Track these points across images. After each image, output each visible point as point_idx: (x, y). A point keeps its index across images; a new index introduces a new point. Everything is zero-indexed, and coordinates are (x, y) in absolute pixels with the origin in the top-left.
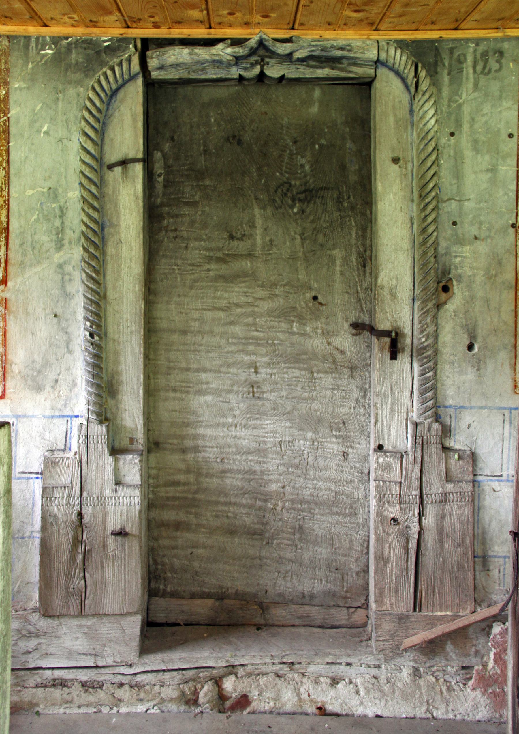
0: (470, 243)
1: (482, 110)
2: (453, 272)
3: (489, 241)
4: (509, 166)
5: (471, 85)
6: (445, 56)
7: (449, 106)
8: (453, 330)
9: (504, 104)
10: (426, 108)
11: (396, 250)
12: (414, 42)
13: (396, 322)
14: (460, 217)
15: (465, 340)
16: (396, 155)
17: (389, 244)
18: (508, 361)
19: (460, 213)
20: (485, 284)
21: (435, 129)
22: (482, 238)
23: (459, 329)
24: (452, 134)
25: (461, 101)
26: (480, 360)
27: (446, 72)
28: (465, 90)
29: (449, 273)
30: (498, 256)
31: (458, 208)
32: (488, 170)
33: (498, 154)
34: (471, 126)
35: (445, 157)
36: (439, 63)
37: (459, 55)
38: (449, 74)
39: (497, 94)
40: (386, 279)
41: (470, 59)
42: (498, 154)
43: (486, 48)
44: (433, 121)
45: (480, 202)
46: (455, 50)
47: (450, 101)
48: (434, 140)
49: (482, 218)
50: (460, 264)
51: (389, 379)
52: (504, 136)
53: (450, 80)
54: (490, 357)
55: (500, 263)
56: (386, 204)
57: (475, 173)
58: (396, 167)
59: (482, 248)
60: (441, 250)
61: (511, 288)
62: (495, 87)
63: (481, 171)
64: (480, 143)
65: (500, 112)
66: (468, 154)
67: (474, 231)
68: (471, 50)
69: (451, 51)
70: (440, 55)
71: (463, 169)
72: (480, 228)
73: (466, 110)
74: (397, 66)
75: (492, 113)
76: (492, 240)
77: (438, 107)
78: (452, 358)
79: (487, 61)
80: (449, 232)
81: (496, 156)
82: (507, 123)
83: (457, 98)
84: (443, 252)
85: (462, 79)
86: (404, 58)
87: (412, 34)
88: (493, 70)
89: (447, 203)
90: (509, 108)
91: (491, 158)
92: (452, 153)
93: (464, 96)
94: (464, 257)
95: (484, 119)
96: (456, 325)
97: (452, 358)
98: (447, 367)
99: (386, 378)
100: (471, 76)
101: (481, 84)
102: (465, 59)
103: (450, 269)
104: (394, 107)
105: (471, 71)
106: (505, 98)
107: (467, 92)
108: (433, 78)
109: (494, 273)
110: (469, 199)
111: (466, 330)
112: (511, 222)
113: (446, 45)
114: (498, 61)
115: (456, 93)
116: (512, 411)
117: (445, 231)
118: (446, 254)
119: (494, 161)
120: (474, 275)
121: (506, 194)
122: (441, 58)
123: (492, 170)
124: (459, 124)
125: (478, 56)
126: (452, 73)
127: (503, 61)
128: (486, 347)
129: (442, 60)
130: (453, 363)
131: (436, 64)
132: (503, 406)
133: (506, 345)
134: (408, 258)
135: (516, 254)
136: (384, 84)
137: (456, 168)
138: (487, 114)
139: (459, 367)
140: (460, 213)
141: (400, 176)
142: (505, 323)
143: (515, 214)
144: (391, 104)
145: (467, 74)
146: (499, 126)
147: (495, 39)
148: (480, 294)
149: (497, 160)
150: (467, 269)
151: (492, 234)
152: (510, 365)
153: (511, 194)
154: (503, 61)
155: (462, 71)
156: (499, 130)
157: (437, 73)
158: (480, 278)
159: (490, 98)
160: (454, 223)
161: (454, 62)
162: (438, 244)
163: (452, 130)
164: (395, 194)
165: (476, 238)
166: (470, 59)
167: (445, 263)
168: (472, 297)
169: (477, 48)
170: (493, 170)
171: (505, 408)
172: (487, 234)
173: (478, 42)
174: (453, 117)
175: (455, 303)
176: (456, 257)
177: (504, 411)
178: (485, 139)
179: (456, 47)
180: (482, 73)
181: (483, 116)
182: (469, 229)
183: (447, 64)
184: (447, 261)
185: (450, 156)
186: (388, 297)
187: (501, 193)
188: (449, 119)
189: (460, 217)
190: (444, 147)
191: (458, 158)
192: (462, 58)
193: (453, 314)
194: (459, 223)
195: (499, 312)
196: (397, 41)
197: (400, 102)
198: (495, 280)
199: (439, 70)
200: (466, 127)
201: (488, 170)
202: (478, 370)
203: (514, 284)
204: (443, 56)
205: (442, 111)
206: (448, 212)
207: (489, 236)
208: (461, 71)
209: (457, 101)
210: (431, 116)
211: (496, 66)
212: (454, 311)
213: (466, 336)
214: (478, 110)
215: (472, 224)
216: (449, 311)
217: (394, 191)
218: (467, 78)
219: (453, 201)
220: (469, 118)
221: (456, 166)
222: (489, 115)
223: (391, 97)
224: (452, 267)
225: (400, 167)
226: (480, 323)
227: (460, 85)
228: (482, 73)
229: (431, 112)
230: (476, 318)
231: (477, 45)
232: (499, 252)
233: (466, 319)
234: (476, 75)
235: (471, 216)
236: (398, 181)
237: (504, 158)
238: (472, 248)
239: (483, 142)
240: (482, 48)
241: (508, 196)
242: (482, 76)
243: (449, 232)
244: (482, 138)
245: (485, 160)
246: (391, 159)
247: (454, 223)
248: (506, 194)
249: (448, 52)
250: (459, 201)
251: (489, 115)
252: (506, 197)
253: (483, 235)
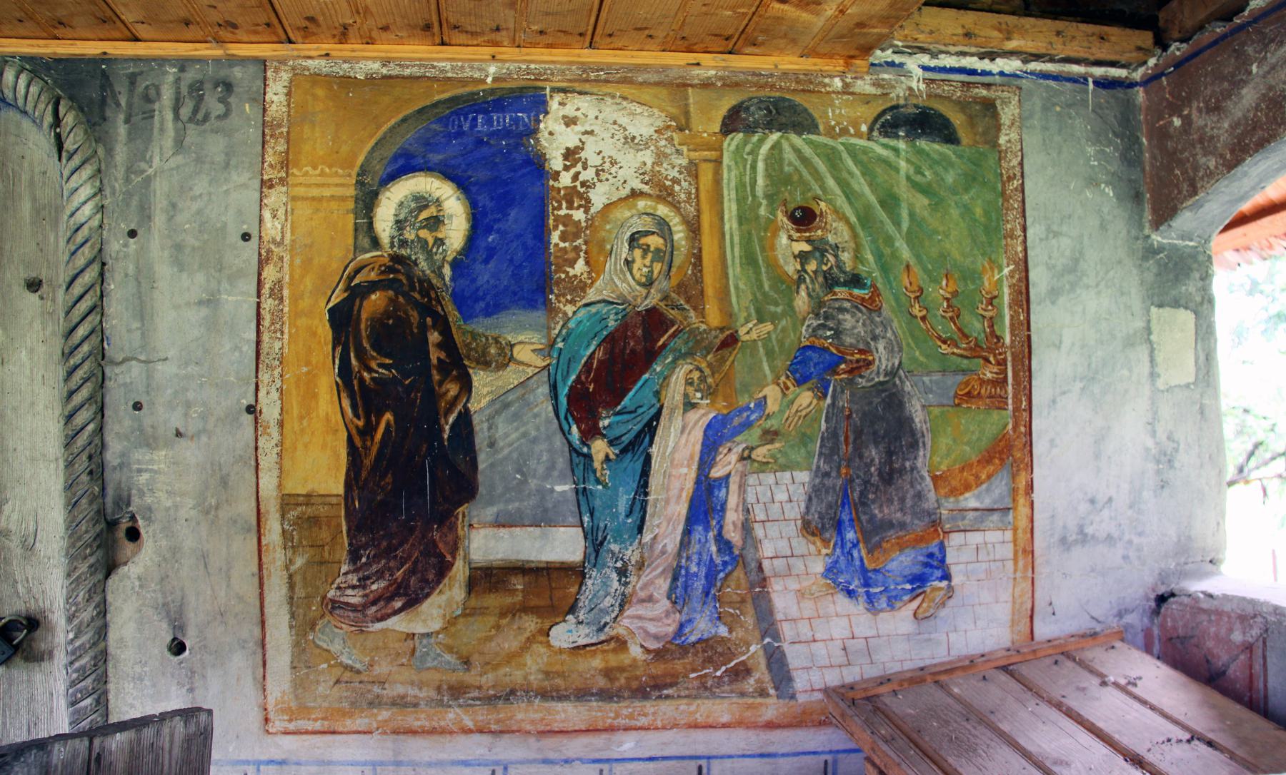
0: (168, 445)
1: (191, 189)
2: (136, 500)
3: (204, 439)
4: (242, 293)
5: (168, 142)
6: (121, 88)
7: (127, 180)
8: (138, 615)
9: (235, 177)
10: (74, 183)
11: (33, 460)
12: (59, 61)
13: (36, 600)
14: (148, 393)
15: (163, 633)
16: (34, 275)
17: (20, 448)
18: (249, 672)
19: (148, 386)
20: (198, 523)
21: (95, 222)
22: (190, 434)
23: (150, 612)
24: (133, 234)
25: (150, 171)
26: (193, 672)
27: (122, 117)
28: (157, 150)
29: (128, 504)
30: (220, 470)
31: (144, 375)
32: (200, 303)
33: (220, 271)
34: (170, 219)
35: (118, 276)
36: (109, 101)
37: (147, 87)
38: (127, 121)
39: (220, 158)
40: (15, 517)
41: (167, 95)
42: (220, 271)
43: (199, 77)
44: (87, 210)
45: (187, 364)
46: (139, 79)
47: (129, 170)
48: (89, 244)
49: (191, 395)
50: (148, 485)
51: (23, 712)
52: (235, 238)
53: (129, 133)
54: (213, 666)
55: (224, 482)
56: (13, 369)
57: (177, 307)
58: (34, 298)
59: (190, 452)
60: (111, 457)
61: (249, 530)
62: (216, 146)
63: (188, 304)
64: (187, 251)
65: (227, 192)
66: (164, 271)
67: (176, 421)
68: (171, 79)
69: (133, 80)
70: (111, 85)
71: (152, 299)
72: (186, 415)
73: (160, 188)
74: (20, 102)
75: (210, 194)
76: (209, 438)
77: (105, 181)
78: (138, 669)
79: (201, 99)
80: (127, 423)
81: (217, 275)
82: (240, 212)
83: (143, 165)
84: (116, 462)
85: (152, 129)
86: (34, 90)
87: (46, 46)
88: (213, 116)
89: (123, 367)
90: (244, 186)
91: (208, 281)
92: (131, 269)
93: (156, 160)
94: (156, 472)
95: (195, 206)
96: (143, 605)
97: (138, 669)
98: (129, 686)
99: (18, 712)
100: (170, 124)
101: (188, 140)
102: (158, 94)
103: (129, 496)
104: (32, 183)
105: (169, 116)
106: (236, 167)
107: (162, 154)
108: (97, 128)
109: (213, 502)
110: (166, 359)
111: (164, 614)
112: (245, 402)
113: (124, 69)
114: (221, 100)
115: (140, 155)
116: (262, 767)
117: (120, 422)
118: (121, 466)
119: (214, 284)
120: (176, 507)
121: (236, 348)
122: (113, 91)
123: (209, 300)
124: (145, 214)
125: (184, 90)
126: (133, 119)
127: (232, 100)
128: (205, 647)
129: (114, 95)
130: (141, 680)
131: (103, 102)
132: (243, 757)
133: (245, 641)
134: (57, 476)
135: (257, 464)
136: (12, 139)
137: (140, 298)
138: (201, 195)
139: (154, 686)
140: (148, 386)
141: (43, 313)
142: (241, 599)
143: (253, 387)
144: (25, 177)
145: (162, 122)
146: (224, 219)
147: (217, 60)
148: (189, 543)
149: (219, 283)
150: (162, 495)
151: (210, 426)
152: (255, 679)
153: (245, 348)
154: (232, 100)
155: (153, 117)
156: (225, 225)
157: (105, 119)
158: (188, 509)
159: (207, 166)
160: (137, 406)
161: (136, 100)
162: (103, 445)
163: (133, 226)
164: (31, 351)
165: (179, 434)
166: (167, 95)
167: (120, 483)
168: (175, 551)
169: (182, 75)
170: (211, 301)
171: (247, 762)
172: (201, 426)
173: (183, 64)
174: (135, 202)
175: (139, 565)
176: (139, 471)
177: (245, 767)
178: (197, 244)
179: (141, 73)
180: (191, 120)
181: (193, 199)
182: (164, 416)
183: (123, 102)
184: (124, 479)
185: (126, 275)
186: (19, 551)
187: (228, 347)
188: (128, 205)
189: (148, 393)
190: (117, 259)
191: (144, 278)
192: (152, 92)
193: (137, 583)
194: (145, 406)
195: (229, 578)
196: (24, 58)
197: (45, 173)
198: (217, 516)
199: (108, 113)
200: (159, 220)
201: (200, 303)
202: (191, 690)
203: (255, 523)
204: (117, 88)
205: (113, 188)
206: (125, 384)
207: (205, 431)
208: (149, 115)
209: (143, 171)
210: (83, 199)
211: (219, 109)
212: (139, 578)
213: (165, 625)
214: (184, 189)
215: (171, 406)
216: (129, 578)
217: (29, 344)
218: (162, 130)
219: (134, 362)
220: (165, 203)
221: (139, 295)
222: (206, 198)
223: (26, 164)
224: (134, 492)
225: (42, 298)
226: (192, 599)
227: (149, 140)
228: (191, 120)
229: (86, 192)
230: (182, 589)
231: (182, 69)
232: (222, 461)
233: (164, 594)
234: (180, 124)
235: (169, 391)
236: (37, 325)
237: (232, 279)
238: (171, 453)
239: (194, 249)
240: (191, 75)
241: (241, 352)
242: (191, 126)
243: (127, 423)
244: (191, 241)
245: (196, 283)
246: (23, 283)
247: (137, 406)
248: (236, 348)
249: (126, 82)
250: (147, 362)
251: (206, 198)
252: (237, 354)
253: (192, 429)
